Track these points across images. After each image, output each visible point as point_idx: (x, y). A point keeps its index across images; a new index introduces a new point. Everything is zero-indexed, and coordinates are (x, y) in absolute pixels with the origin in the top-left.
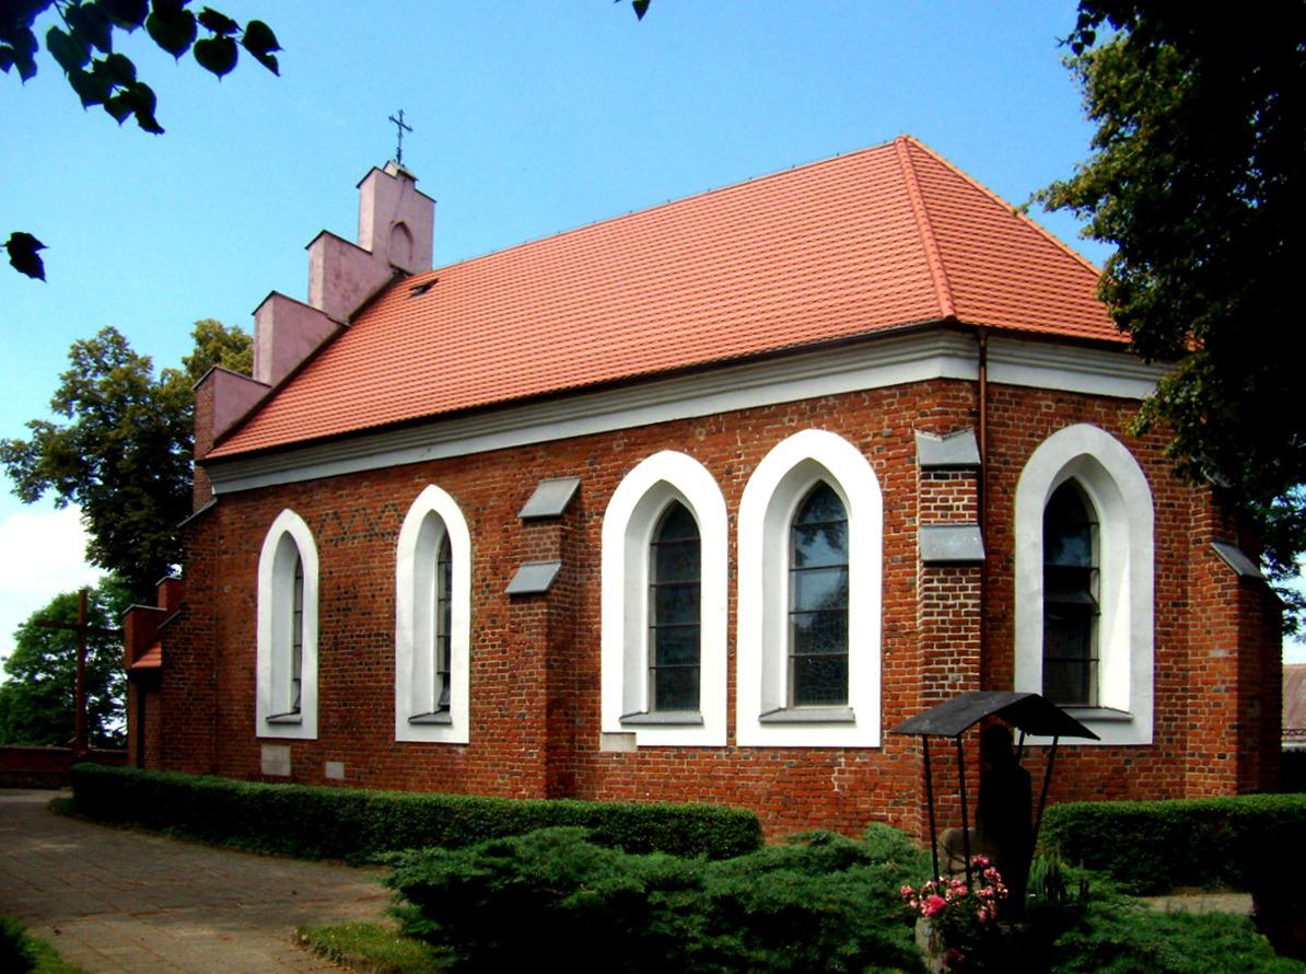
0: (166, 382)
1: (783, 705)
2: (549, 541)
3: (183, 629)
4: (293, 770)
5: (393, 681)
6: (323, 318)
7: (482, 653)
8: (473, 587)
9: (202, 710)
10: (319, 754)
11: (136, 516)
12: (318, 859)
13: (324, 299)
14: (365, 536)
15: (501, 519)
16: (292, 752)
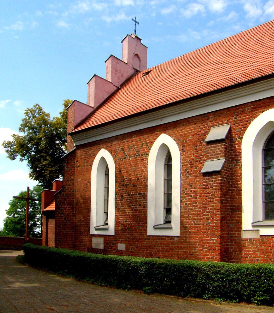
0: (54, 121)
1: (261, 220)
2: (219, 150)
3: (63, 195)
4: (104, 246)
5: (147, 212)
6: (112, 85)
7: (185, 199)
8: (181, 173)
9: (70, 224)
10: (115, 240)
11: (44, 163)
12: (130, 289)
13: (112, 78)
14: (134, 156)
15: (194, 145)
16: (104, 240)
